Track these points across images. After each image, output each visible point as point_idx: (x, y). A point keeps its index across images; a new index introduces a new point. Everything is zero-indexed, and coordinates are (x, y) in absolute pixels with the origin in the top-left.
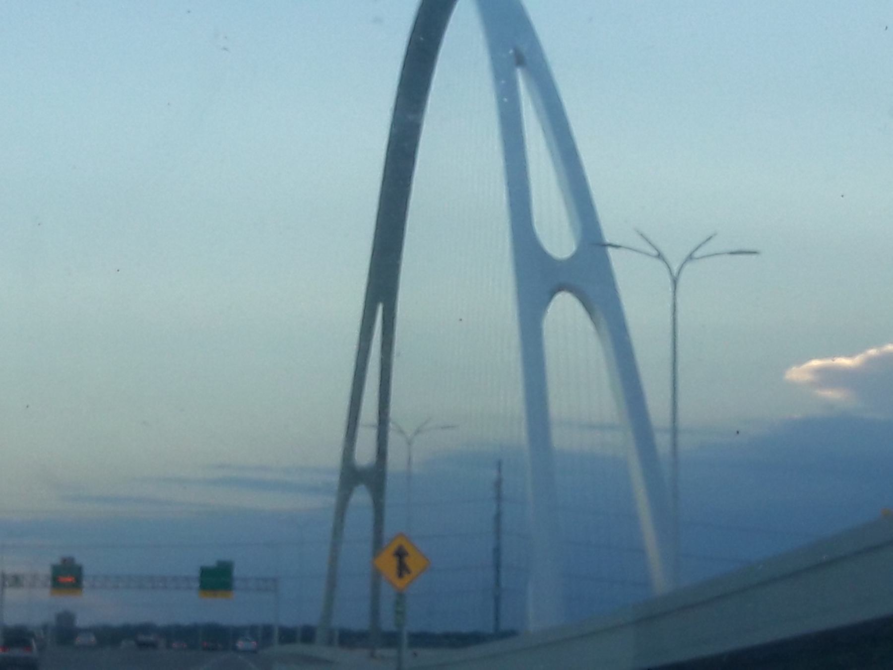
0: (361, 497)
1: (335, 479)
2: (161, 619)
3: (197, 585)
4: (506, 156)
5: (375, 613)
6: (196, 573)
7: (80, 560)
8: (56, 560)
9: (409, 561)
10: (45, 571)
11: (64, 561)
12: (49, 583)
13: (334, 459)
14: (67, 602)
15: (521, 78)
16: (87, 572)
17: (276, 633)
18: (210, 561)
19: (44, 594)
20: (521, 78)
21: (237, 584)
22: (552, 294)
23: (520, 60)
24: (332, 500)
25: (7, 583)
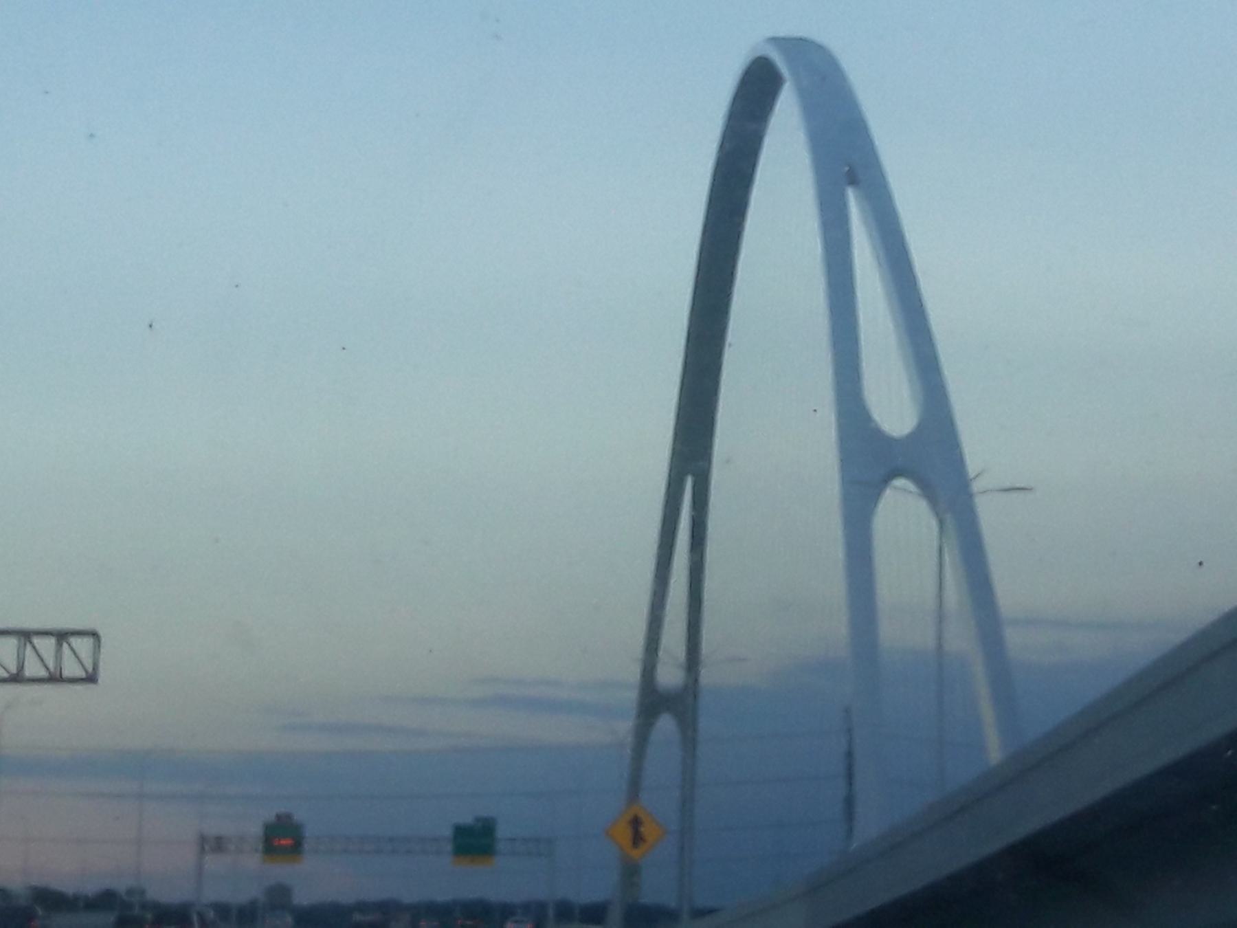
0: (666, 724)
1: (631, 697)
2: (411, 893)
3: (449, 847)
4: (691, 566)
5: (631, 872)
6: (448, 832)
7: (299, 815)
8: (269, 815)
9: (646, 830)
10: (255, 830)
11: (278, 817)
12: (261, 847)
13: (633, 673)
14: (281, 872)
15: (853, 200)
16: (309, 832)
17: (551, 913)
18: (467, 819)
19: (252, 861)
20: (853, 200)
21: (501, 846)
22: (886, 480)
23: (852, 179)
24: (625, 727)
25: (207, 848)
